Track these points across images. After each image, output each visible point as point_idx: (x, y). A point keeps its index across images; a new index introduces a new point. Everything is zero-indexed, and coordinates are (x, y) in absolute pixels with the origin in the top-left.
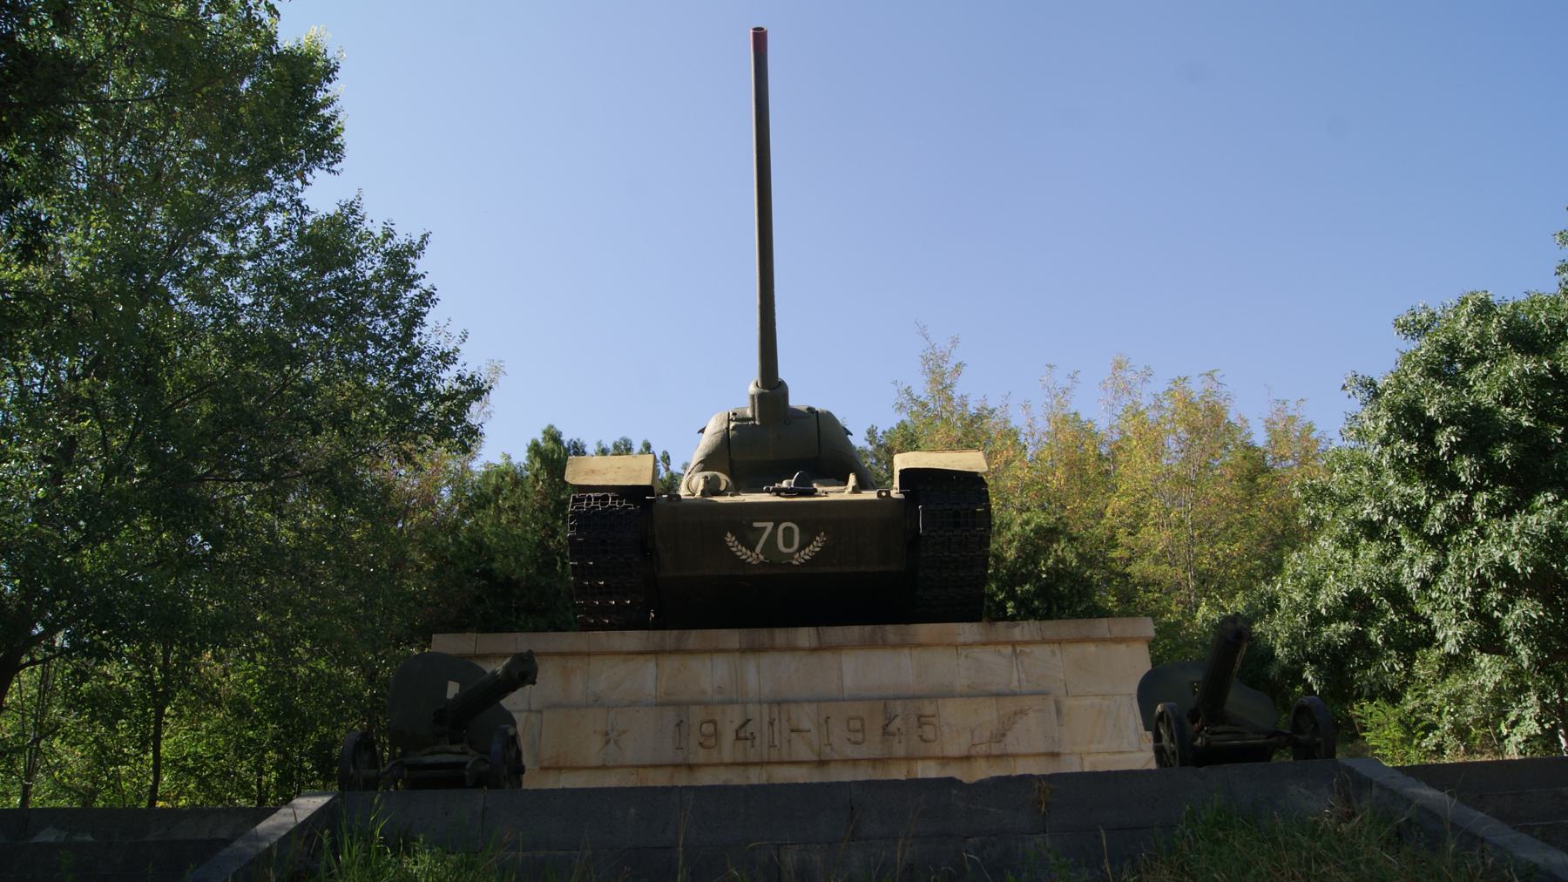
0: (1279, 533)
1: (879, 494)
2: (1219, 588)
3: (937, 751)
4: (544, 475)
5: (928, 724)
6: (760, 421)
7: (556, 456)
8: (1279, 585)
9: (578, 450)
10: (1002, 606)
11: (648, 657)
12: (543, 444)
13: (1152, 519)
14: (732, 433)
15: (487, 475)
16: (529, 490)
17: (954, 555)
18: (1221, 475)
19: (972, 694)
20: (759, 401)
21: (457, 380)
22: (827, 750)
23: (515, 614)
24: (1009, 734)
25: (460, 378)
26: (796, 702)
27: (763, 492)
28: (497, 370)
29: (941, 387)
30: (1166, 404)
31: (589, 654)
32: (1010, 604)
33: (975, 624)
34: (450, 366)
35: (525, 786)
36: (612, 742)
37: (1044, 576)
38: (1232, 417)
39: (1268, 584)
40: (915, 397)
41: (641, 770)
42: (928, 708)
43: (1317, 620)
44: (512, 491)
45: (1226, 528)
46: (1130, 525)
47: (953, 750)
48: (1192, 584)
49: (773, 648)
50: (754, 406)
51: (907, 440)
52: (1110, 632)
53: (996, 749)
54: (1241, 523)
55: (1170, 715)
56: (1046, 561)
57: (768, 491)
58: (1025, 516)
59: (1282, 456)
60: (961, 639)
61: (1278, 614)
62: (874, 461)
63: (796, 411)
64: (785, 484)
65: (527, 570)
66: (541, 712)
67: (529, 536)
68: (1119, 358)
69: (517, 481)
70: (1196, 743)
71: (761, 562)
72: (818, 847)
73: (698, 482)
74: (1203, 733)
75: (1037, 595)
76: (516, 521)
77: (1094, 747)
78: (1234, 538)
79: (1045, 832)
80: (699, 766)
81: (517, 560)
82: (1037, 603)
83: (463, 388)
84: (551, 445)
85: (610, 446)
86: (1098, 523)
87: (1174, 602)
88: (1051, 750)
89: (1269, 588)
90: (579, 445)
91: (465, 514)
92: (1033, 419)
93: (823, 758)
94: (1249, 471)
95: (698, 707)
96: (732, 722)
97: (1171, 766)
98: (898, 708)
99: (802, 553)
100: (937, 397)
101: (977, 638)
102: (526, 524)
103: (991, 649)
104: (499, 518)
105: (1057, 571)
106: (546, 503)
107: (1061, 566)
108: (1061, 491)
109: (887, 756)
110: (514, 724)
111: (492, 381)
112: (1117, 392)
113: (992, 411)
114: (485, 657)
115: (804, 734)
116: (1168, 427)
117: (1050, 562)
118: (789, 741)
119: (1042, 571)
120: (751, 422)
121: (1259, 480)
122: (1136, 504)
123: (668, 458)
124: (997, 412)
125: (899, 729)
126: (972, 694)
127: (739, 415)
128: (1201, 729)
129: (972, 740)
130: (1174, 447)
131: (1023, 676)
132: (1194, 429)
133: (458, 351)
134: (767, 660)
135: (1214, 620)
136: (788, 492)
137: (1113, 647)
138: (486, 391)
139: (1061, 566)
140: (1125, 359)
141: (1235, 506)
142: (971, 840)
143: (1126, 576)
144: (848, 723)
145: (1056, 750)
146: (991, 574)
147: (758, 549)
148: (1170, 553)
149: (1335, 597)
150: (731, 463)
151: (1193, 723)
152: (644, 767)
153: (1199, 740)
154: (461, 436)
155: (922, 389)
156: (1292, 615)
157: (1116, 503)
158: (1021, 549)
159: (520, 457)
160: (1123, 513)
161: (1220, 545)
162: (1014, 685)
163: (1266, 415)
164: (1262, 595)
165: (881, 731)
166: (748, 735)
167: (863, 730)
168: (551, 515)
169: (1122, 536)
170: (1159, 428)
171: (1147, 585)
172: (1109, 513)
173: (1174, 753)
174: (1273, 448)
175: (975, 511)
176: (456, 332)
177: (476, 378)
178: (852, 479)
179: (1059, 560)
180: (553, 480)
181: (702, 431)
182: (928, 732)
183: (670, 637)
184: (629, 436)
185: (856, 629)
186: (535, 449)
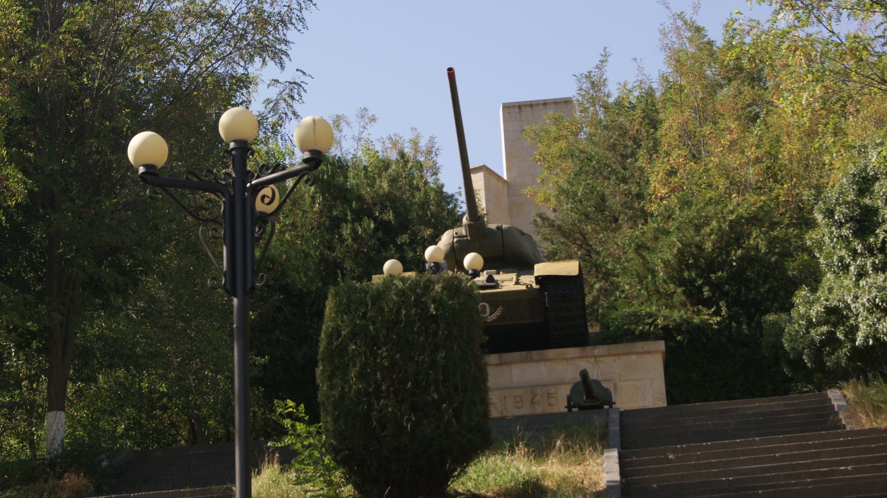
5: (553, 397)
6: (470, 237)
14: (455, 245)
32: (706, 288)
37: (735, 264)
42: (553, 390)
43: (810, 325)
52: (642, 348)
60: (569, 356)
119: (733, 260)
127: (459, 234)
146: (692, 264)
149: (818, 311)
167: (522, 402)
168: (327, 230)
182: (553, 401)
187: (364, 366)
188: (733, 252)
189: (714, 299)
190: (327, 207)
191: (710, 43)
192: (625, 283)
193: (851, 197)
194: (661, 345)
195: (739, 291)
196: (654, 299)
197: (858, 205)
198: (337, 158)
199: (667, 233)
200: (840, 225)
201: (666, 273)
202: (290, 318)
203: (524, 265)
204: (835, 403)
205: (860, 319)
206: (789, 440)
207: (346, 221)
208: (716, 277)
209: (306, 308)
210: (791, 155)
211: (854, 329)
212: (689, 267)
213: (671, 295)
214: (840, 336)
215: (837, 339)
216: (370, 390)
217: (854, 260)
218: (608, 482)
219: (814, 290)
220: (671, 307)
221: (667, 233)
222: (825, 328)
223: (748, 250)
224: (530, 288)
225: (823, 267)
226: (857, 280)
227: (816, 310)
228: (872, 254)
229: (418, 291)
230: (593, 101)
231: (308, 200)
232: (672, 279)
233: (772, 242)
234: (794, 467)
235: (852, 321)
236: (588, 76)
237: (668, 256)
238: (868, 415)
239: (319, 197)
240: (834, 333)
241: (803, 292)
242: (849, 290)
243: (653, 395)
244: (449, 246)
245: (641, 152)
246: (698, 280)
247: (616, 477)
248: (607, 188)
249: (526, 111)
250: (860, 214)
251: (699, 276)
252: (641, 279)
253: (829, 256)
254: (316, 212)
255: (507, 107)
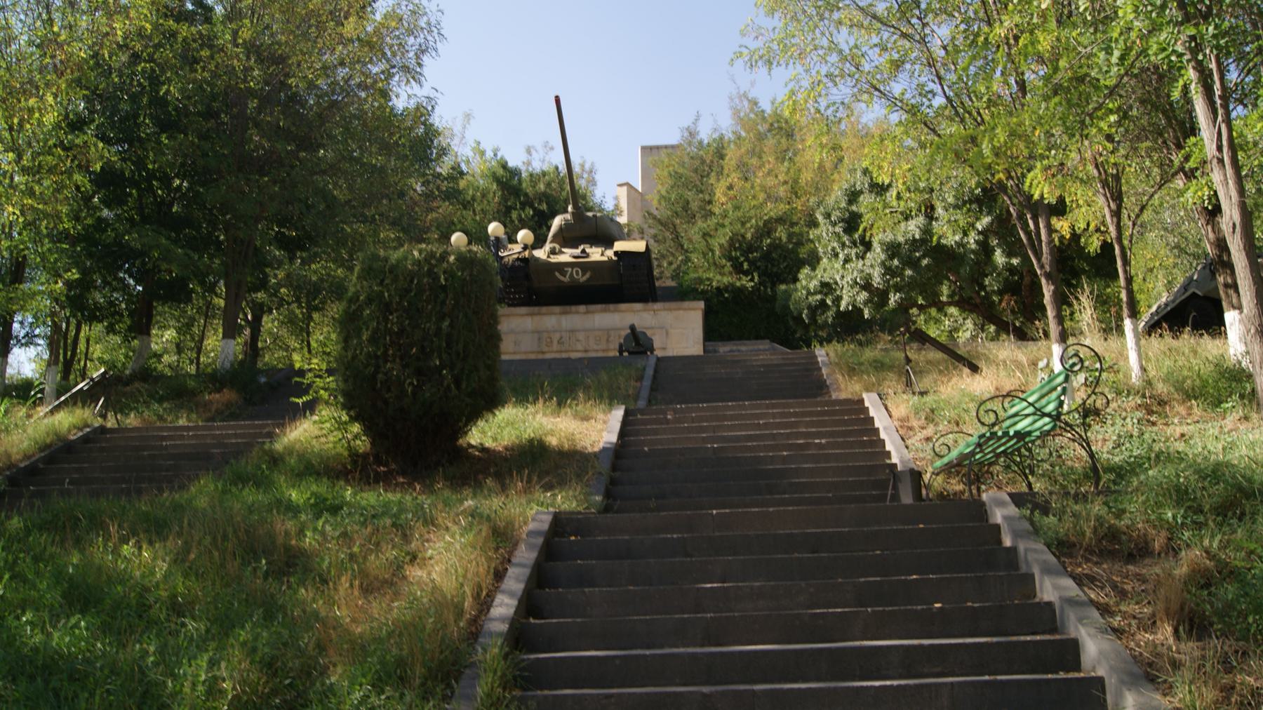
43: (809, 293)
187: (375, 331)
190: (504, 199)
191: (763, 111)
192: (695, 258)
193: (843, 205)
194: (701, 304)
195: (767, 266)
196: (713, 268)
197: (848, 210)
199: (723, 226)
200: (834, 224)
201: (721, 252)
203: (607, 242)
204: (819, 359)
205: (844, 292)
206: (774, 406)
207: (515, 209)
210: (807, 181)
211: (839, 299)
212: (736, 249)
213: (723, 267)
214: (829, 302)
215: (827, 304)
216: (379, 353)
217: (843, 250)
218: (606, 443)
219: (814, 269)
220: (722, 274)
221: (723, 226)
222: (819, 297)
223: (775, 240)
224: (610, 260)
225: (821, 254)
226: (844, 264)
227: (813, 284)
228: (856, 246)
229: (433, 262)
230: (690, 144)
231: (492, 195)
232: (724, 256)
233: (790, 236)
234: (774, 437)
235: (838, 293)
236: (687, 129)
237: (723, 241)
238: (843, 375)
240: (825, 301)
241: (806, 270)
242: (838, 271)
245: (713, 174)
247: (613, 438)
248: (690, 195)
249: (654, 151)
250: (849, 217)
251: (741, 255)
252: (705, 255)
253: (825, 246)
255: (644, 148)
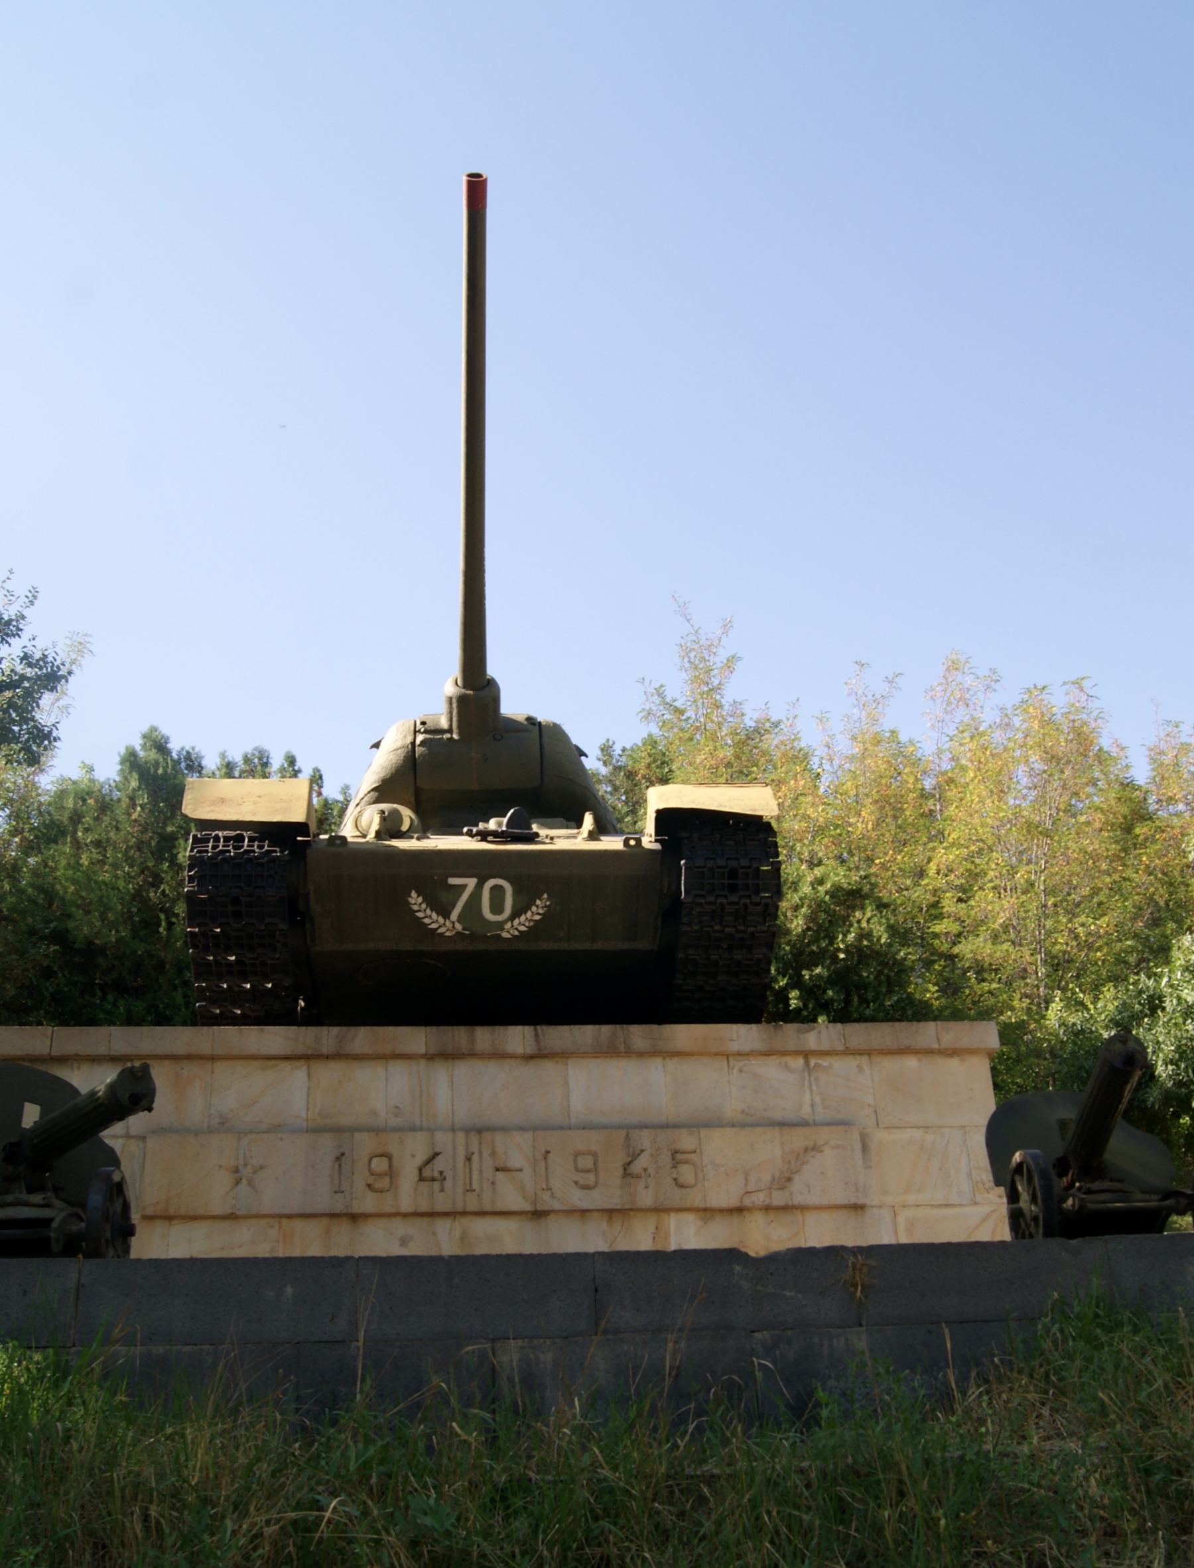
0: (1162, 903)
1: (626, 842)
2: (1078, 977)
3: (698, 1202)
4: (142, 799)
5: (687, 1162)
6: (460, 734)
7: (160, 771)
8: (1165, 980)
9: (193, 764)
10: (782, 996)
11: (298, 1063)
12: (142, 754)
13: (991, 881)
14: (419, 751)
15: (61, 794)
16: (122, 818)
17: (727, 930)
18: (1088, 823)
19: (747, 1123)
20: (459, 706)
21: (22, 659)
22: (546, 1196)
23: (99, 994)
24: (797, 1178)
25: (25, 658)
26: (505, 1129)
27: (461, 834)
28: (81, 647)
29: (706, 689)
30: (1017, 721)
31: (213, 1058)
32: (794, 994)
33: (753, 1026)
34: (11, 640)
35: (133, 1255)
36: (244, 1181)
37: (842, 956)
38: (1105, 742)
39: (1149, 978)
40: (668, 700)
41: (284, 1221)
42: (686, 1141)
44: (97, 819)
45: (1091, 896)
46: (962, 889)
47: (722, 1197)
48: (1042, 971)
49: (472, 1055)
50: (451, 713)
51: (655, 761)
53: (778, 1199)
54: (1111, 889)
55: (1031, 1163)
56: (845, 935)
57: (470, 834)
58: (818, 872)
59: (1170, 799)
60: (735, 1047)
61: (1162, 1017)
62: (609, 789)
63: (511, 724)
64: (492, 825)
65: (117, 931)
66: (143, 1138)
67: (121, 884)
68: (954, 657)
69: (105, 806)
70: (1065, 1206)
71: (458, 933)
72: (548, 1342)
73: (371, 819)
74: (1073, 1191)
75: (832, 981)
76: (102, 862)
77: (911, 1198)
78: (1101, 910)
79: (861, 1325)
80: (366, 1216)
81: (103, 918)
82: (830, 993)
83: (29, 672)
84: (153, 755)
85: (238, 758)
86: (917, 884)
87: (1017, 996)
88: (853, 1201)
89: (1151, 983)
90: (193, 757)
91: (28, 848)
92: (832, 737)
93: (540, 1208)
94: (1125, 817)
95: (366, 1134)
96: (413, 1156)
97: (1031, 1236)
98: (645, 1139)
99: (516, 922)
100: (699, 704)
101: (756, 1045)
102: (116, 866)
103: (774, 1060)
104: (77, 857)
105: (860, 950)
106: (146, 837)
107: (865, 943)
108: (869, 838)
109: (627, 1206)
110: (117, 1163)
111: (73, 662)
112: (949, 703)
113: (776, 725)
114: (63, 1060)
115: (515, 1173)
116: (1018, 753)
117: (851, 937)
118: (493, 1183)
119: (839, 950)
120: (447, 736)
121: (1137, 831)
122: (970, 858)
123: (321, 777)
124: (782, 726)
125: (645, 1170)
126: (747, 1123)
127: (430, 725)
128: (1072, 1185)
129: (746, 1185)
130: (1025, 781)
131: (817, 1099)
132: (1052, 758)
133: (23, 617)
134: (463, 1070)
135: (1074, 1024)
136: (498, 836)
137: (941, 1061)
138: (63, 677)
139: (865, 943)
140: (962, 659)
141: (1104, 866)
142: (756, 1334)
143: (951, 958)
144: (575, 1161)
145: (860, 1201)
147: (454, 915)
148: (1014, 928)
150: (418, 792)
151: (1060, 1176)
152: (290, 1217)
153: (1070, 1202)
154: (27, 741)
155: (679, 689)
156: (1180, 1020)
157: (943, 856)
158: (812, 918)
159: (108, 771)
160: (951, 871)
161: (1083, 918)
162: (806, 1111)
163: (1151, 741)
164: (1141, 992)
165: (620, 1172)
166: (436, 1174)
169: (949, 904)
170: (1005, 755)
171: (981, 970)
172: (932, 869)
173: (1035, 1219)
174: (1159, 786)
175: (758, 869)
176: (21, 589)
177: (50, 659)
178: (588, 820)
179: (864, 935)
180: (156, 805)
181: (377, 745)
182: (686, 1173)
183: (328, 1036)
184: (266, 746)
185: (589, 1030)
186: (131, 761)
188: (841, 936)
189: (805, 1013)
198: (184, 753)
202: (66, 989)
208: (811, 976)
209: (98, 975)
239: (143, 795)
243: (970, 1174)
244: (401, 754)
246: (780, 978)
254: (135, 821)
